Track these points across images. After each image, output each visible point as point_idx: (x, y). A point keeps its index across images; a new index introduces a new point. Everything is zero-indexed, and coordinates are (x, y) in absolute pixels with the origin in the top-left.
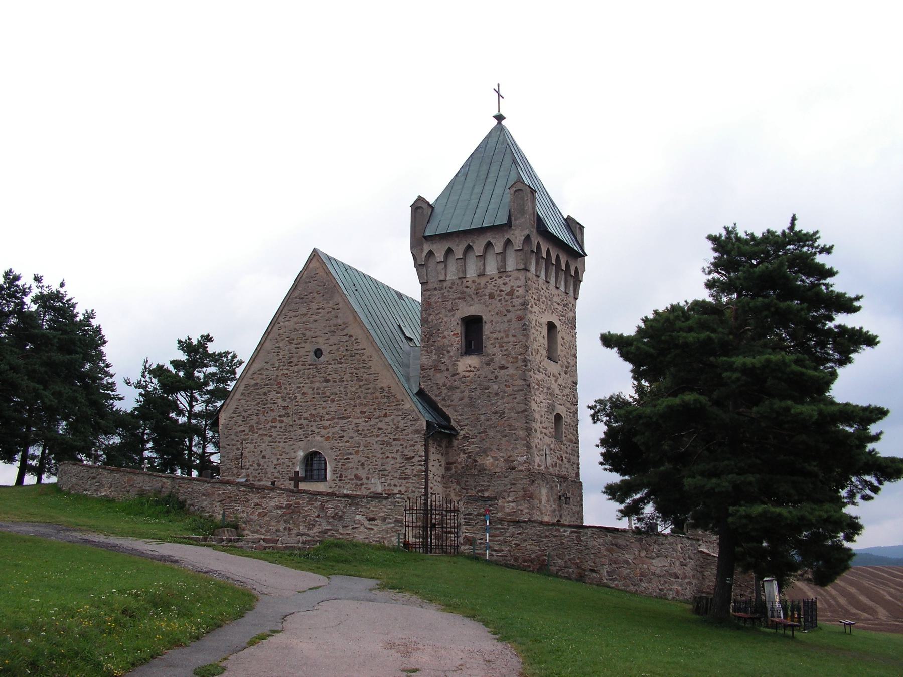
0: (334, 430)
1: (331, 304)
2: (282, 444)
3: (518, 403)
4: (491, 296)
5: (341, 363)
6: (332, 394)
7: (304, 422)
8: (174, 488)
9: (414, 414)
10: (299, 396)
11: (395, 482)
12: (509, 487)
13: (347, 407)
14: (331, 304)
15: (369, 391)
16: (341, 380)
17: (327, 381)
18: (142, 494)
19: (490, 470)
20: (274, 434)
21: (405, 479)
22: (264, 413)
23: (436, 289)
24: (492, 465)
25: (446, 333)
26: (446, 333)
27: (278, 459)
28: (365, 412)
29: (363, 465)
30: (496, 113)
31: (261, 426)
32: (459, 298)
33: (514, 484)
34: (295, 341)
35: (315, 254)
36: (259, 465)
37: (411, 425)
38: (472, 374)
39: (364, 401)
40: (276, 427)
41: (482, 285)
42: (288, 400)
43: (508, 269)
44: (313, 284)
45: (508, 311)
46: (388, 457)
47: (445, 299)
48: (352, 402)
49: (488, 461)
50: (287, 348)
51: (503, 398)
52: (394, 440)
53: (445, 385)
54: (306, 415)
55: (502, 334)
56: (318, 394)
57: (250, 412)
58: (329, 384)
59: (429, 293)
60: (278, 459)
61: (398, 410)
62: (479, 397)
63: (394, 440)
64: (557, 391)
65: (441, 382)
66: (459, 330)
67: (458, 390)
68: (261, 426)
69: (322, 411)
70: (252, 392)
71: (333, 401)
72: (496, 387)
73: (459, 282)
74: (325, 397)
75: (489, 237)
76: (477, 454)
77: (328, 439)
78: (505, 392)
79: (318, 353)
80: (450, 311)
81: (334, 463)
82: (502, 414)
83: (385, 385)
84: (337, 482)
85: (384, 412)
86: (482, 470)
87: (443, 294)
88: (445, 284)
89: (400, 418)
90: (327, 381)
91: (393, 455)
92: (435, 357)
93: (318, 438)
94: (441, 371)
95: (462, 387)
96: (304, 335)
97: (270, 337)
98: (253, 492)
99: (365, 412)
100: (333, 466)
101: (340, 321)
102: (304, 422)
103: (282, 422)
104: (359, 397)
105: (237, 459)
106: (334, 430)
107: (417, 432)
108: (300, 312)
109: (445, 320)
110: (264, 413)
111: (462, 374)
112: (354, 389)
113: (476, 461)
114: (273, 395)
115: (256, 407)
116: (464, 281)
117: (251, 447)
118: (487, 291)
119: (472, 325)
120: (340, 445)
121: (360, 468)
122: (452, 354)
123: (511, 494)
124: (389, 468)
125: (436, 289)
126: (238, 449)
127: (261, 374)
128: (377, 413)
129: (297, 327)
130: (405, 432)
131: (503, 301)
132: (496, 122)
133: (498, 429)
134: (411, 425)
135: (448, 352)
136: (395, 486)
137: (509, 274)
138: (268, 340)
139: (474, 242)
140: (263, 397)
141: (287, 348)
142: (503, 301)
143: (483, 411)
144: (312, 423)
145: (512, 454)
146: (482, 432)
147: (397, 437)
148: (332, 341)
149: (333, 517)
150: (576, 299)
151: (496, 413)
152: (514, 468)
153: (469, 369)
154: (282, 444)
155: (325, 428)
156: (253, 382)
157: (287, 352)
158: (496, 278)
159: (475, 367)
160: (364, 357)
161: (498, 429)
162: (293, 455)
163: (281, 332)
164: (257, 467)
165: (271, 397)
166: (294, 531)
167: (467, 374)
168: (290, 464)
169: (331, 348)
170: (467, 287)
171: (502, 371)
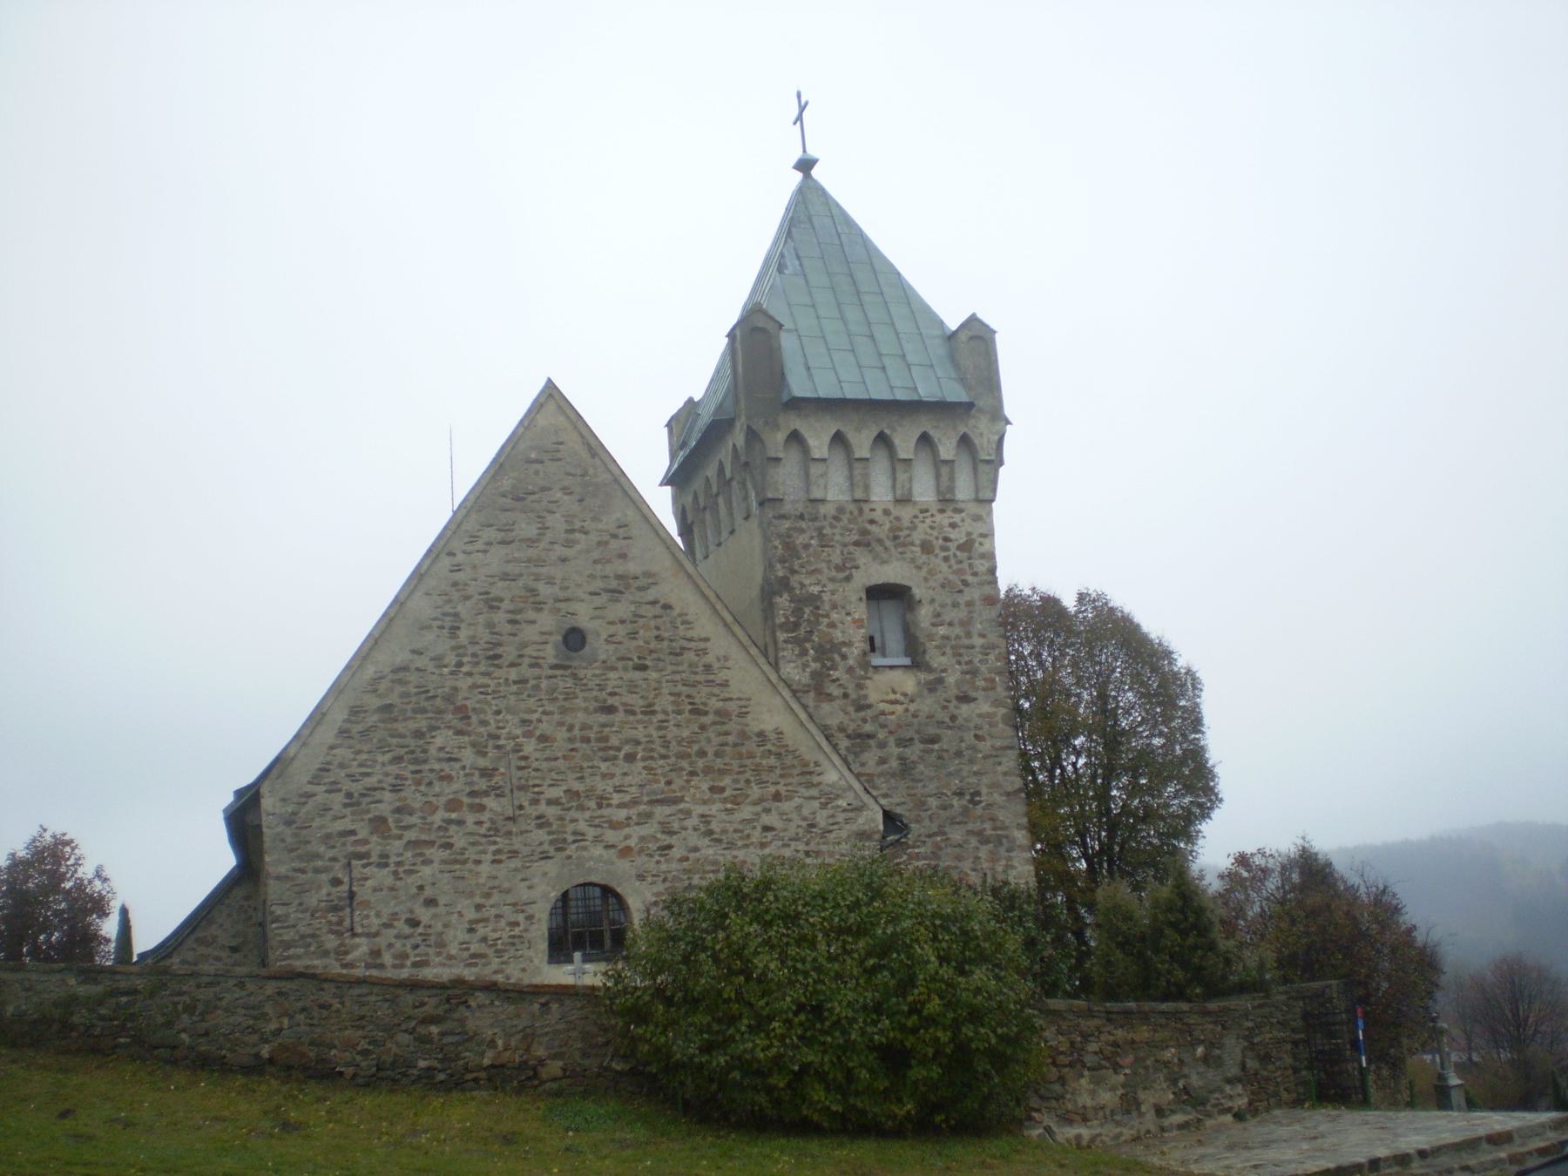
3: (1005, 774)
4: (926, 547)
5: (644, 668)
7: (552, 812)
13: (673, 775)
15: (731, 739)
16: (649, 711)
17: (610, 710)
20: (459, 842)
23: (801, 517)
25: (835, 616)
27: (479, 907)
28: (722, 790)
30: (797, 154)
31: (414, 820)
32: (857, 544)
35: (551, 395)
36: (414, 923)
37: (847, 821)
38: (899, 708)
40: (460, 823)
41: (906, 522)
42: (492, 753)
45: (965, 583)
50: (481, 619)
51: (971, 761)
52: (807, 854)
55: (958, 630)
56: (587, 740)
57: (371, 781)
61: (810, 785)
63: (807, 854)
67: (872, 742)
68: (414, 820)
69: (602, 786)
71: (630, 758)
73: (852, 507)
74: (607, 752)
77: (626, 852)
79: (574, 639)
85: (772, 789)
88: (822, 509)
89: (816, 804)
90: (610, 710)
93: (598, 851)
94: (830, 698)
95: (881, 735)
96: (533, 591)
99: (722, 790)
101: (632, 568)
102: (552, 812)
104: (702, 753)
105: (336, 909)
107: (863, 835)
116: (866, 507)
118: (917, 537)
120: (664, 867)
125: (801, 517)
131: (953, 562)
132: (799, 176)
134: (847, 821)
137: (961, 505)
139: (893, 430)
142: (953, 562)
144: (573, 814)
146: (935, 834)
147: (813, 847)
153: (892, 697)
155: (615, 826)
158: (933, 510)
159: (905, 695)
162: (525, 895)
165: (439, 741)
168: (521, 918)
169: (612, 629)
170: (872, 522)
171: (965, 709)
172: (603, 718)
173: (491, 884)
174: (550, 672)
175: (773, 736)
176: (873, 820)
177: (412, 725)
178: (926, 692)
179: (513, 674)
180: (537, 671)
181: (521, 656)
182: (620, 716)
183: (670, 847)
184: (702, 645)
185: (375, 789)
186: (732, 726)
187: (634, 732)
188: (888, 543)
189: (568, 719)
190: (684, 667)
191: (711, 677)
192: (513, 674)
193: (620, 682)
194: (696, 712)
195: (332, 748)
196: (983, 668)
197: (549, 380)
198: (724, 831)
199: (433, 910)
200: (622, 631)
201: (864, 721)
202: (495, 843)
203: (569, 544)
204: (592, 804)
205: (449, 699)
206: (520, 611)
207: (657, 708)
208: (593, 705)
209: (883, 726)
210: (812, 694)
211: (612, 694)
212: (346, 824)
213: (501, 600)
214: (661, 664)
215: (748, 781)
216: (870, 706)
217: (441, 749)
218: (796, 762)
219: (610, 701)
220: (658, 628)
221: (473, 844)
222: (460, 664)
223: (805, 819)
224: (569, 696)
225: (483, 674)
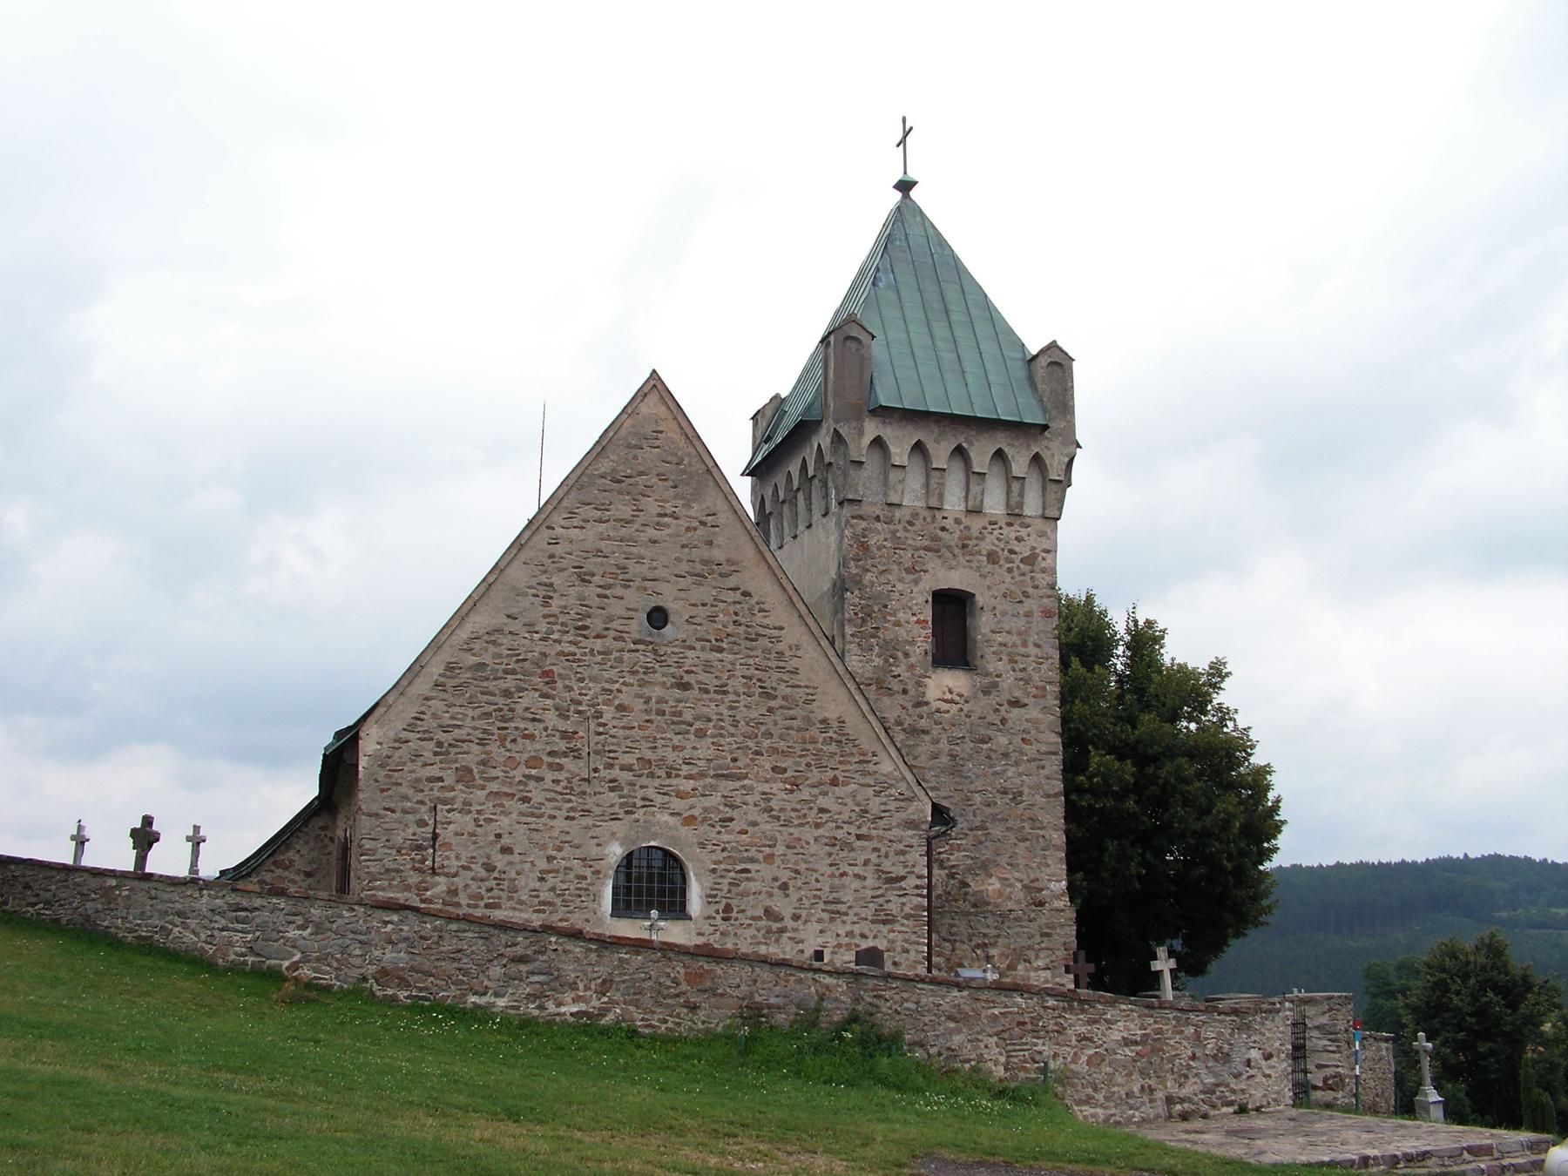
0: (706, 802)
1: (696, 510)
2: (560, 824)
4: (992, 558)
5: (721, 650)
6: (697, 718)
8: (857, 1000)
9: (903, 787)
10: (609, 713)
11: (864, 927)
14: (696, 510)
15: (795, 723)
17: (685, 686)
18: (753, 1013)
19: (996, 905)
20: (537, 796)
21: (884, 922)
22: (503, 740)
23: (878, 519)
24: (1000, 894)
25: (901, 615)
26: (901, 615)
27: (550, 859)
28: (785, 770)
29: (784, 887)
30: (899, 176)
32: (927, 549)
33: (1048, 935)
34: (597, 579)
36: (490, 868)
37: (898, 809)
38: (955, 708)
39: (782, 745)
40: (540, 779)
42: (575, 717)
43: (1027, 512)
44: (649, 455)
46: (844, 874)
48: (750, 744)
49: (993, 886)
50: (572, 591)
52: (859, 837)
53: (899, 723)
56: (661, 713)
57: (457, 733)
59: (864, 524)
60: (550, 859)
61: (865, 773)
62: (971, 758)
63: (859, 837)
65: (891, 716)
66: (927, 614)
67: (927, 738)
68: (494, 773)
69: (671, 756)
70: (465, 685)
71: (701, 734)
72: (1003, 740)
76: (969, 870)
78: (1022, 753)
79: (658, 617)
81: (709, 880)
82: (1017, 796)
83: (831, 715)
84: (719, 921)
85: (831, 774)
86: (980, 903)
87: (894, 532)
88: (898, 513)
89: (870, 791)
90: (685, 686)
91: (857, 870)
92: (878, 661)
95: (936, 730)
97: (523, 556)
98: (1071, 1008)
99: (785, 770)
100: (708, 885)
101: (717, 554)
102: (625, 776)
103: (560, 767)
104: (769, 735)
105: (419, 848)
106: (706, 802)
107: (911, 824)
108: (613, 513)
109: (900, 587)
110: (503, 740)
111: (935, 705)
112: (754, 714)
113: (965, 885)
114: (529, 699)
115: (481, 723)
116: (939, 515)
117: (466, 822)
118: (985, 547)
119: (952, 609)
120: (725, 837)
122: (913, 660)
123: (1042, 954)
124: (848, 897)
125: (878, 519)
126: (422, 823)
127: (494, 643)
128: (815, 775)
130: (881, 823)
131: (1016, 573)
132: (898, 195)
133: (1010, 824)
134: (898, 809)
135: (907, 655)
136: (863, 936)
137: (1028, 521)
138: (516, 562)
139: (971, 444)
140: (501, 701)
142: (1016, 573)
143: (978, 785)
145: (1038, 874)
146: (977, 828)
147: (864, 831)
149: (1215, 1057)
151: (1005, 792)
153: (948, 696)
154: (560, 824)
155: (681, 795)
156: (472, 660)
157: (572, 601)
159: (960, 695)
161: (1010, 824)
162: (594, 852)
163: (558, 550)
165: (525, 702)
166: (1159, 1095)
167: (944, 706)
169: (694, 611)
170: (943, 529)
171: (1016, 711)
172: (677, 693)
178: (980, 695)
179: (598, 645)
180: (620, 645)
183: (732, 820)
184: (776, 633)
188: (956, 551)
189: (646, 691)
190: (758, 653)
194: (768, 696)
196: (1036, 677)
198: (782, 810)
199: (508, 857)
202: (570, 801)
204: (661, 773)
206: (609, 587)
207: (729, 688)
208: (670, 681)
210: (873, 688)
212: (434, 771)
215: (809, 765)
217: (527, 709)
218: (855, 750)
219: (686, 678)
220: (736, 614)
221: (550, 800)
223: (859, 805)
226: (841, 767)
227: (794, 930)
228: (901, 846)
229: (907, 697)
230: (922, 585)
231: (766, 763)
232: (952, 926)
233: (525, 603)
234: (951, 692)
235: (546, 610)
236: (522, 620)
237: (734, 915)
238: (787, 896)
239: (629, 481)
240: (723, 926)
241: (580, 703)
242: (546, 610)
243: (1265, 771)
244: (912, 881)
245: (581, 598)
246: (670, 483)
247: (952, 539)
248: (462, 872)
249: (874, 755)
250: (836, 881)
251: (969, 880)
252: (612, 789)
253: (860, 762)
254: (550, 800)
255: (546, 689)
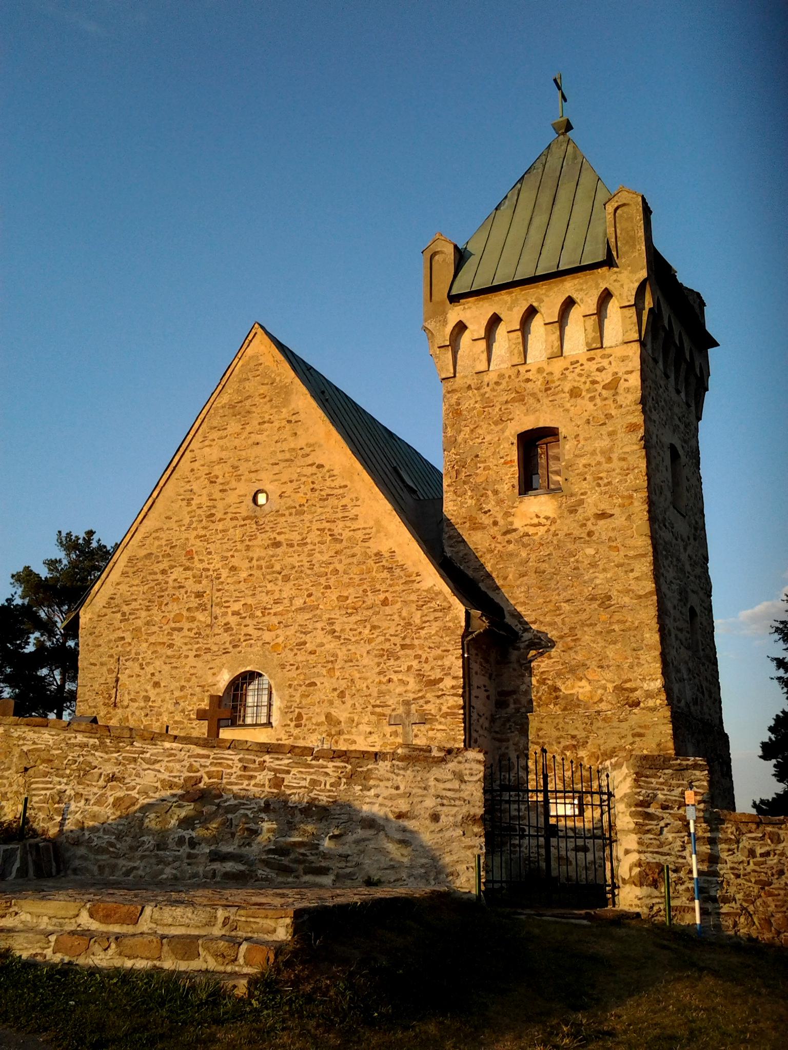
2: (191, 661)
3: (637, 579)
7: (233, 620)
10: (224, 573)
12: (630, 739)
15: (355, 560)
17: (277, 544)
20: (178, 639)
23: (469, 387)
33: (640, 735)
36: (147, 699)
37: (436, 619)
38: (542, 530)
40: (180, 630)
45: (609, 416)
46: (390, 681)
47: (488, 403)
50: (204, 492)
54: (236, 607)
56: (260, 568)
58: (279, 551)
59: (455, 396)
63: (403, 647)
64: (688, 568)
69: (265, 598)
71: (286, 579)
75: (569, 287)
76: (559, 674)
80: (496, 423)
82: (605, 601)
85: (382, 596)
86: (571, 704)
90: (277, 544)
94: (482, 527)
101: (301, 442)
103: (193, 619)
111: (522, 530)
112: (325, 558)
113: (556, 689)
118: (567, 387)
119: (534, 444)
121: (337, 702)
122: (501, 495)
125: (469, 387)
127: (157, 538)
129: (224, 455)
130: (423, 633)
135: (496, 492)
139: (541, 301)
140: (160, 577)
141: (204, 492)
142: (598, 401)
147: (408, 641)
148: (285, 477)
150: (699, 418)
151: (593, 599)
152: (637, 704)
153: (536, 521)
156: (143, 552)
159: (547, 518)
160: (344, 501)
164: (142, 704)
165: (173, 577)
170: (528, 380)
172: (270, 552)
173: (192, 671)
174: (243, 523)
175: (387, 555)
176: (456, 618)
177: (162, 566)
178: (566, 514)
180: (235, 522)
181: (226, 513)
182: (284, 548)
183: (305, 643)
185: (138, 610)
186: (357, 550)
187: (291, 559)
189: (250, 554)
190: (328, 509)
191: (346, 514)
192: (220, 526)
193: (285, 525)
194: (336, 540)
195: (118, 584)
197: (717, 345)
199: (157, 690)
200: (289, 488)
201: (509, 542)
202: (198, 643)
203: (260, 432)
204: (259, 613)
205: (183, 546)
207: (308, 540)
209: (525, 546)
211: (279, 534)
213: (217, 478)
214: (313, 509)
216: (515, 530)
217: (175, 580)
218: (402, 574)
219: (279, 538)
220: (313, 483)
221: (186, 644)
222: (191, 523)
223: (404, 619)
224: (252, 537)
225: (205, 528)
226: (391, 589)
227: (349, 732)
228: (439, 652)
229: (496, 528)
230: (507, 433)
231: (333, 595)
232: (540, 729)
233: (175, 506)
234: (538, 516)
235: (189, 509)
236: (175, 518)
237: (303, 722)
238: (344, 703)
239: (240, 405)
240: (296, 732)
241: (208, 570)
242: (189, 509)
243: (771, 729)
244: (448, 682)
245: (210, 495)
246: (268, 398)
247: (538, 385)
248: (132, 704)
249: (418, 575)
250: (384, 687)
251: (559, 684)
252: (226, 631)
253: (405, 583)
254: (186, 644)
255: (188, 564)
